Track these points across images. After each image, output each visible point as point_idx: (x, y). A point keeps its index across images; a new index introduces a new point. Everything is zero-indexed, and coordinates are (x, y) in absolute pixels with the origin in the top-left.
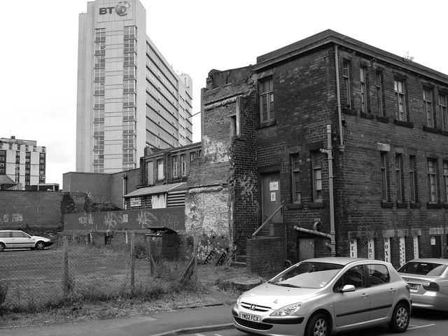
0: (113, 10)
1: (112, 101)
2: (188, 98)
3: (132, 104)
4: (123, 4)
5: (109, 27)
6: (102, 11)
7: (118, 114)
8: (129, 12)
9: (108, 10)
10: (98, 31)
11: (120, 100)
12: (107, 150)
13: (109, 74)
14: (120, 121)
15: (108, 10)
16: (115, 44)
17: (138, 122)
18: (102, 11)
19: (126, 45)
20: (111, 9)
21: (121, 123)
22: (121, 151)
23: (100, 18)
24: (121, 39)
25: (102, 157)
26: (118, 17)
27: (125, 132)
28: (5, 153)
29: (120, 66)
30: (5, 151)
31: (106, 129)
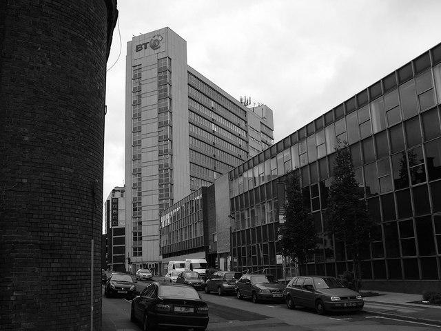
0: (148, 45)
1: (148, 136)
2: (265, 129)
3: (166, 122)
4: (156, 38)
5: (144, 63)
6: (138, 48)
7: (153, 149)
8: (162, 45)
9: (143, 46)
10: (135, 68)
11: (155, 163)
12: (144, 187)
13: (146, 164)
14: (155, 155)
15: (143, 46)
16: (150, 75)
17: (174, 154)
18: (138, 48)
19: (160, 78)
20: (145, 44)
21: (156, 158)
22: (157, 187)
23: (136, 55)
24: (155, 72)
25: (140, 194)
26: (152, 52)
27: (160, 166)
28: (117, 201)
29: (155, 99)
30: (117, 199)
31: (143, 137)
